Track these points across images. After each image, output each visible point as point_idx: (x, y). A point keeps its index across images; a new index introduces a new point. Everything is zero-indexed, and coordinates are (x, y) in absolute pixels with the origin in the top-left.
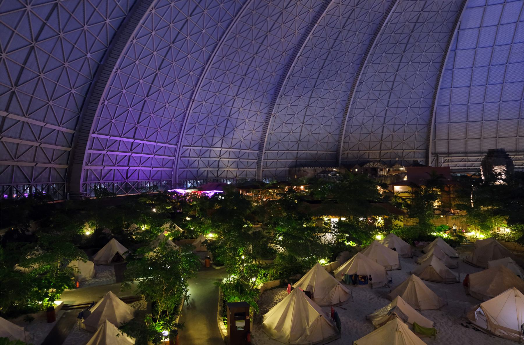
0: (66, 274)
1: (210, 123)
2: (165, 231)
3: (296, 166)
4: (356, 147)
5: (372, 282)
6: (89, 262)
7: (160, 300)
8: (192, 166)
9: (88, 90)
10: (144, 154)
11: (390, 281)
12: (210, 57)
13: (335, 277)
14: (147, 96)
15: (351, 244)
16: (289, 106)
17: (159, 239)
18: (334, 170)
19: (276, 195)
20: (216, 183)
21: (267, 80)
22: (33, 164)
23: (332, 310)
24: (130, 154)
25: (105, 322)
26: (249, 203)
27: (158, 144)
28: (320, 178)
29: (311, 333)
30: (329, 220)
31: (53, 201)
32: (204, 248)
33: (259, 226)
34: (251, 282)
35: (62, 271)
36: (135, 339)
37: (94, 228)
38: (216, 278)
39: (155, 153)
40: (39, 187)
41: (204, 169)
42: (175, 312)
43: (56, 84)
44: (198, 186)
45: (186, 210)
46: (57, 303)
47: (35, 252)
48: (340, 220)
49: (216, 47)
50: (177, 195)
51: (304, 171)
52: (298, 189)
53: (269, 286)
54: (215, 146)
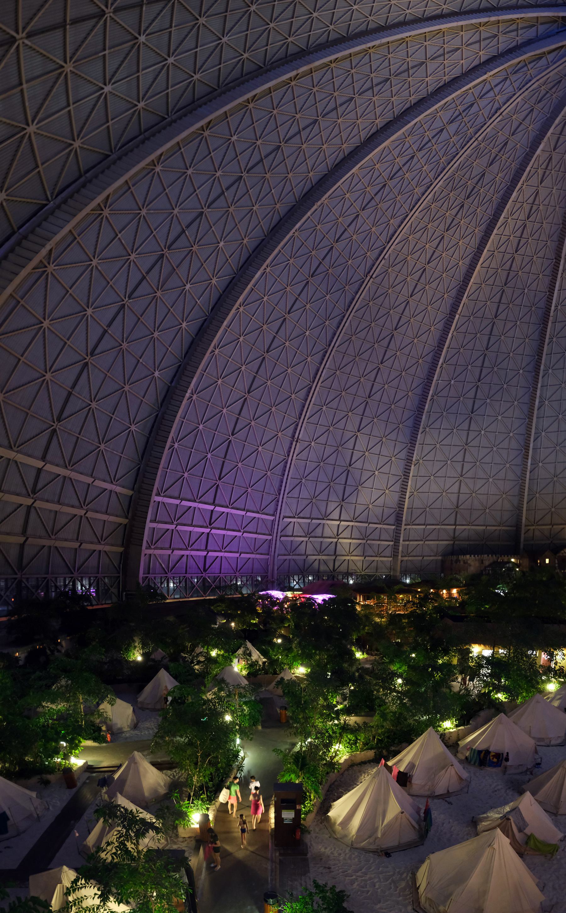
1: (322, 477)
3: (453, 553)
4: (547, 519)
5: (509, 763)
8: (297, 552)
9: (153, 427)
11: (538, 764)
12: (318, 370)
14: (233, 435)
15: (501, 696)
16: (438, 446)
18: (513, 560)
20: (330, 581)
21: (402, 403)
22: (76, 545)
24: (207, 530)
27: (249, 514)
29: (383, 835)
38: (289, 741)
39: (242, 528)
43: (112, 418)
49: (325, 356)
51: (465, 562)
54: (331, 517)
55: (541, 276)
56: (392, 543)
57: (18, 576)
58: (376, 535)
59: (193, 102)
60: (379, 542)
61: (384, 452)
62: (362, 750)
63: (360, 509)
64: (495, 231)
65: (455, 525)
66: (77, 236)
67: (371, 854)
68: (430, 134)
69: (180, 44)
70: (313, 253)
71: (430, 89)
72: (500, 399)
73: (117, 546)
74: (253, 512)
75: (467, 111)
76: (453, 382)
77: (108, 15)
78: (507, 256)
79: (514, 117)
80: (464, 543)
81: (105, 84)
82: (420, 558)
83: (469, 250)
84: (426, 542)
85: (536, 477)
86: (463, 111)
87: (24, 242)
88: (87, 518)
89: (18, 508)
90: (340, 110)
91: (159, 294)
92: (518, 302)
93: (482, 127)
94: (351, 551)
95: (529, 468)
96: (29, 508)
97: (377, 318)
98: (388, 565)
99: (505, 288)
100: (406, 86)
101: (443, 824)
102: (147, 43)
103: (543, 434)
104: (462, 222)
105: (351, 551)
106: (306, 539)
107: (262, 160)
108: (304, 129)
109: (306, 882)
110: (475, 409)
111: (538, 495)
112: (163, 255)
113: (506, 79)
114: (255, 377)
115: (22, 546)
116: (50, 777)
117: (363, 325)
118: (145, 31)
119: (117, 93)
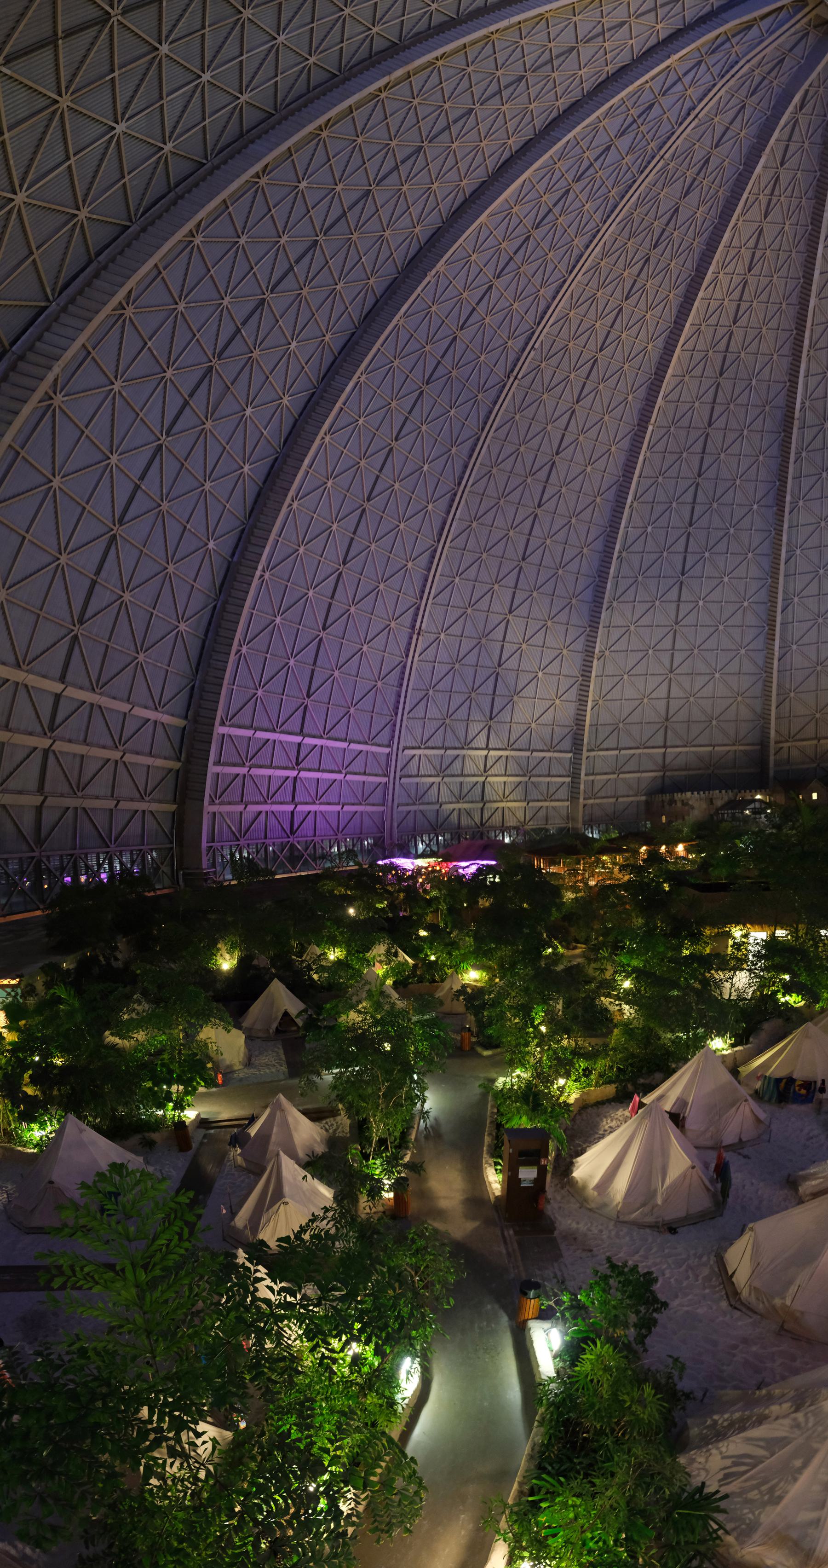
0: (196, 1055)
2: (377, 964)
3: (662, 790)
6: (235, 1031)
7: (375, 1116)
9: (210, 624)
10: (324, 771)
12: (444, 523)
13: (739, 1083)
14: (324, 629)
15: (794, 1000)
16: (632, 628)
17: (367, 983)
18: (758, 797)
19: (620, 870)
20: (478, 841)
21: (573, 567)
23: (719, 1157)
24: (294, 773)
25: (278, 1155)
26: (556, 892)
28: (723, 820)
29: (665, 1201)
30: (746, 936)
31: (154, 890)
32: (459, 1006)
33: (578, 951)
34: (555, 1086)
35: (189, 1048)
36: (332, 1191)
37: (237, 954)
38: (482, 1075)
39: (344, 767)
40: (126, 858)
41: (451, 806)
42: (403, 1143)
44: (441, 850)
45: (419, 911)
46: (190, 1115)
47: (135, 1006)
48: (773, 936)
49: (453, 500)
50: (397, 873)
51: (684, 803)
52: (670, 852)
53: (593, 1098)
54: (473, 745)
55: (775, 357)
56: (568, 779)
57: (36, 854)
58: (543, 768)
59: (242, 135)
60: (548, 779)
61: (551, 641)
62: (597, 1085)
63: (517, 730)
64: (701, 294)
65: (665, 746)
66: (91, 350)
67: (648, 1231)
68: (590, 155)
69: (218, 52)
70: (428, 348)
71: (587, 87)
72: (725, 551)
73: (167, 802)
74: (359, 743)
75: (644, 115)
76: (649, 529)
77: (115, 19)
78: (721, 331)
79: (716, 120)
80: (676, 773)
81: (117, 122)
82: (613, 800)
83: (662, 326)
84: (621, 776)
85: (789, 668)
86: (639, 117)
87: (21, 365)
88: (124, 763)
89: (31, 753)
90: (454, 130)
91: (209, 425)
92: (743, 400)
93: (669, 138)
94: (507, 794)
95: (777, 654)
96: (46, 752)
97: (528, 438)
98: (564, 813)
99: (721, 380)
100: (550, 85)
101: (744, 1186)
102: (171, 55)
103: (796, 599)
104: (648, 284)
105: (507, 794)
106: (438, 779)
107: (344, 214)
108: (403, 162)
109: (561, 1270)
110: (687, 569)
111: (792, 694)
112: (211, 367)
113: (699, 63)
114: (352, 539)
115: (39, 809)
116: (156, 1136)
117: (508, 449)
118: (167, 37)
119: (134, 134)
